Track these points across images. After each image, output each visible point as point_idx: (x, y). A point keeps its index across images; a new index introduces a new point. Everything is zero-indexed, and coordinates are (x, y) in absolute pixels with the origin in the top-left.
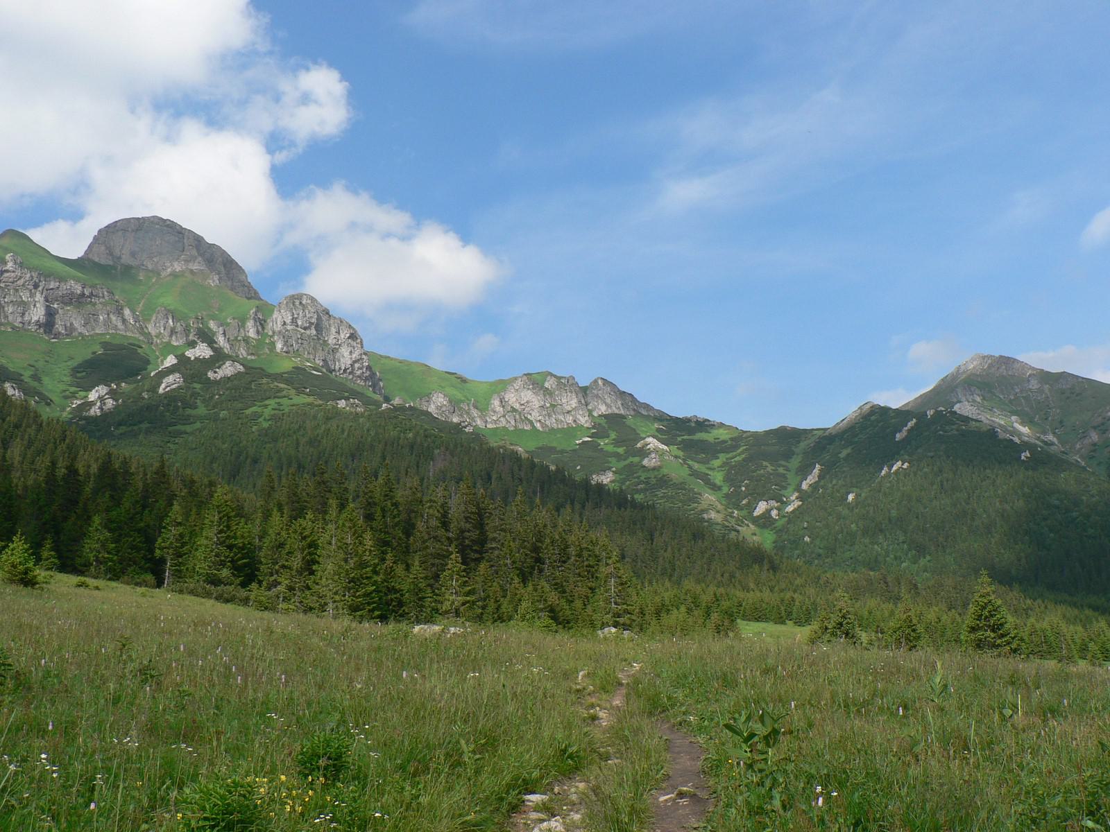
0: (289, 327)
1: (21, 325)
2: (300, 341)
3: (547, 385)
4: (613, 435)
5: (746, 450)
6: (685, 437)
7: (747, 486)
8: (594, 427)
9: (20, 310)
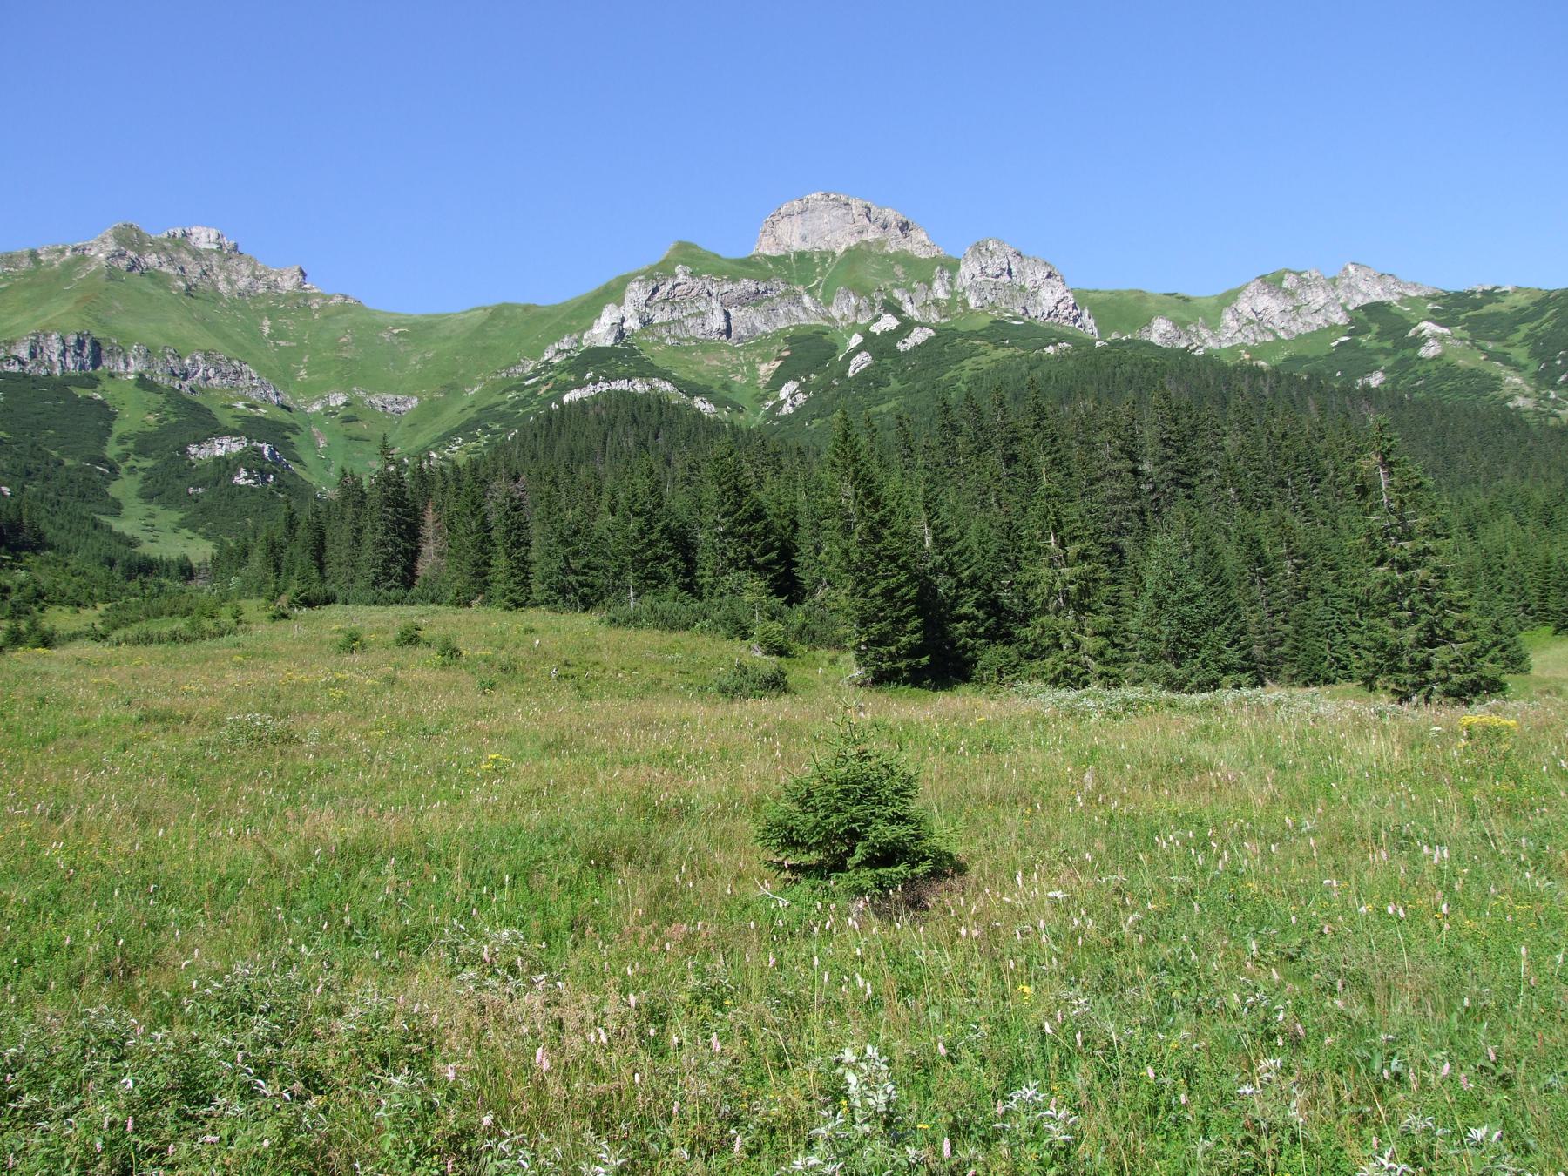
4: (1375, 328)
5: (1556, 313)
6: (1470, 313)
8: (1350, 323)
9: (699, 321)
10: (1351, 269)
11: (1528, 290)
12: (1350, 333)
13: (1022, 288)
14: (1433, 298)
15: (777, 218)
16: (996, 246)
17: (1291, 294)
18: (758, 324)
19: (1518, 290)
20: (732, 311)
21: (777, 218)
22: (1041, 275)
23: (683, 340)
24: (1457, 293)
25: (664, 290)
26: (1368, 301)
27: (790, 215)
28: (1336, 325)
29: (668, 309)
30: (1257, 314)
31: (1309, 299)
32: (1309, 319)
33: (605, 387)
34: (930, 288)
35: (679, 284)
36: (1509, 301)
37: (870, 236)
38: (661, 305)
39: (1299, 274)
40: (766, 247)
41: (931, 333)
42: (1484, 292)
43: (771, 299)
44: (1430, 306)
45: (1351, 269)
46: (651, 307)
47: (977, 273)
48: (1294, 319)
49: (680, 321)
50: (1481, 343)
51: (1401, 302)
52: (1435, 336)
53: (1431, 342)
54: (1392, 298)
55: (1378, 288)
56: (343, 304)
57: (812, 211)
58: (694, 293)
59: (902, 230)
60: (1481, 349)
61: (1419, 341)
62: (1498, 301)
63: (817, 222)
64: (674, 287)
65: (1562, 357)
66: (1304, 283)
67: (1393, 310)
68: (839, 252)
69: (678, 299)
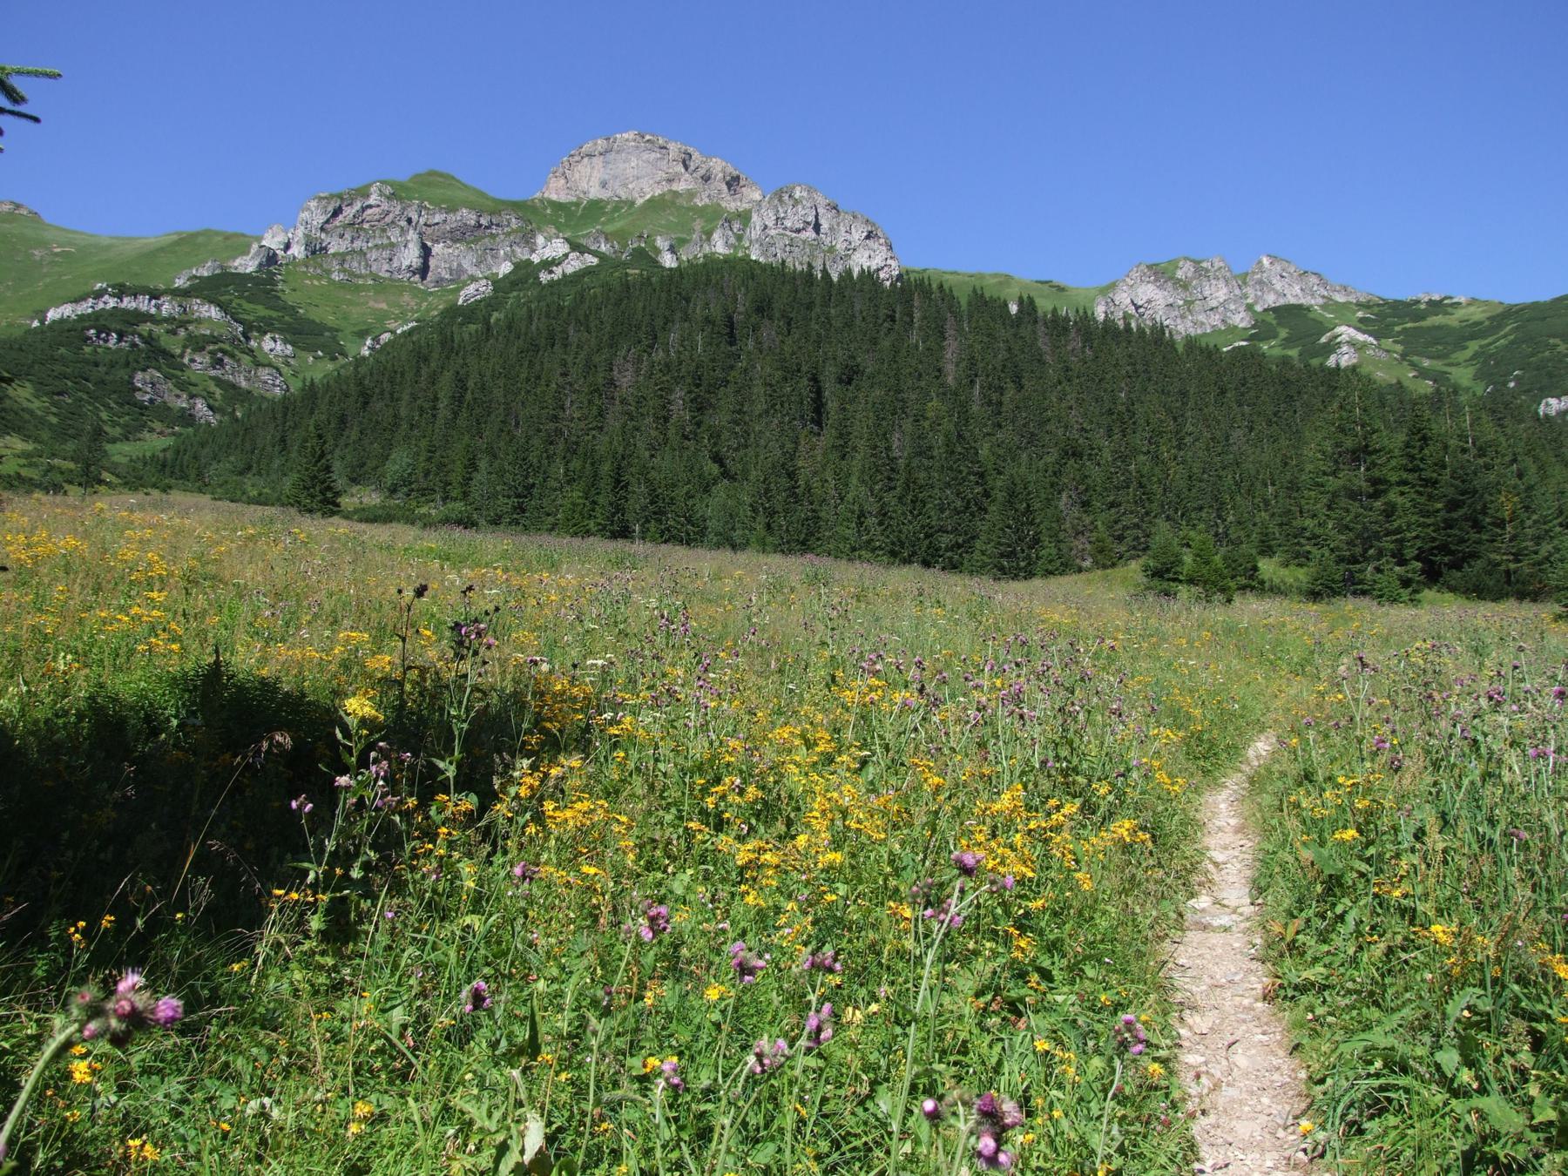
0: (773, 232)
1: (387, 275)
2: (788, 249)
3: (1179, 274)
4: (1283, 333)
5: (1517, 328)
6: (1409, 325)
7: (1517, 379)
8: (1253, 327)
9: (386, 254)
10: (1266, 261)
11: (1486, 303)
12: (1251, 338)
13: (832, 249)
14: (1360, 305)
15: (577, 158)
16: (805, 194)
17: (1185, 286)
18: (466, 265)
19: (1473, 302)
20: (437, 249)
21: (577, 158)
22: (858, 235)
23: (360, 276)
24: (1396, 301)
25: (349, 212)
26: (1282, 302)
27: (590, 156)
28: (1236, 327)
29: (348, 236)
30: (1137, 307)
31: (1207, 293)
32: (1202, 318)
33: (112, 303)
34: (709, 239)
35: (370, 206)
36: (1460, 313)
37: (680, 187)
38: (340, 230)
39: (1197, 263)
40: (556, 191)
41: (595, 261)
42: (1431, 303)
43: (493, 236)
44: (1360, 314)
45: (1266, 261)
46: (327, 233)
47: (770, 223)
48: (1183, 317)
49: (362, 253)
50: (1415, 358)
51: (1323, 307)
52: (1352, 343)
53: (1345, 349)
54: (1315, 302)
55: (1297, 288)
56: (10, 213)
57: (618, 152)
58: (388, 219)
59: (729, 185)
60: (1413, 365)
61: (1331, 347)
62: (1446, 313)
63: (622, 166)
64: (364, 209)
65: (1517, 379)
66: (1201, 272)
67: (1311, 315)
68: (640, 202)
69: (366, 226)
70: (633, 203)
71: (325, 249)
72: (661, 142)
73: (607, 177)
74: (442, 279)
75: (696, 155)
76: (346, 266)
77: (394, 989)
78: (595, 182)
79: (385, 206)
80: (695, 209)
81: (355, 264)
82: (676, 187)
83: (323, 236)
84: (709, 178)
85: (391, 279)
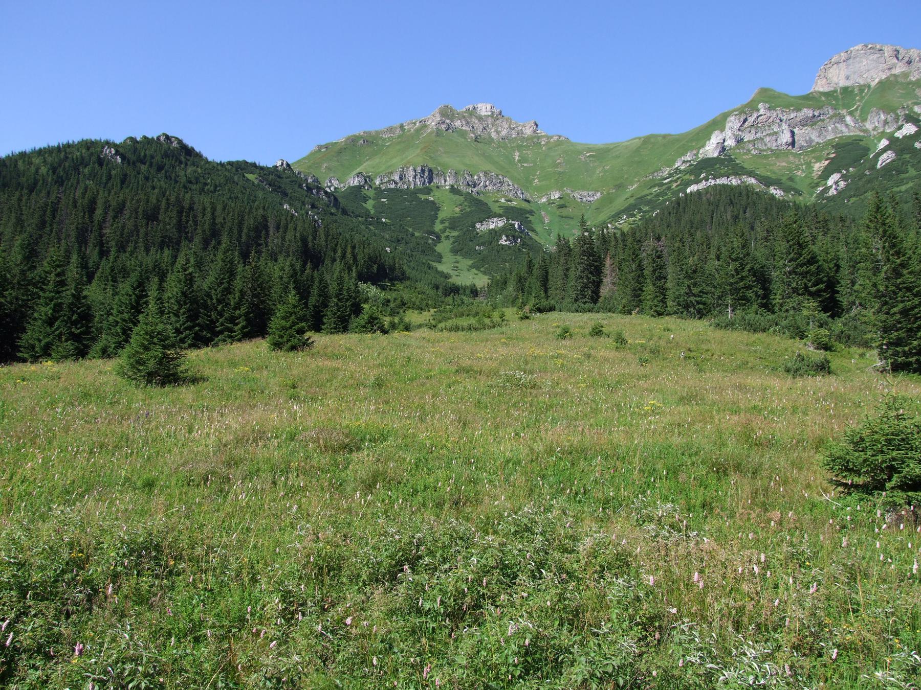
9: (774, 138)
15: (828, 66)
20: (796, 130)
25: (751, 120)
27: (838, 63)
29: (753, 131)
33: (713, 182)
35: (761, 115)
37: (897, 71)
40: (821, 86)
43: (823, 120)
46: (742, 131)
49: (762, 139)
57: (854, 58)
58: (771, 120)
64: (758, 117)
70: (869, 86)
71: (742, 139)
72: (878, 47)
73: (849, 73)
74: (803, 146)
75: (902, 51)
76: (756, 146)
77: (729, 493)
78: (842, 77)
79: (768, 114)
80: (911, 83)
81: (760, 145)
82: (894, 72)
83: (740, 133)
84: (911, 62)
85: (777, 150)
